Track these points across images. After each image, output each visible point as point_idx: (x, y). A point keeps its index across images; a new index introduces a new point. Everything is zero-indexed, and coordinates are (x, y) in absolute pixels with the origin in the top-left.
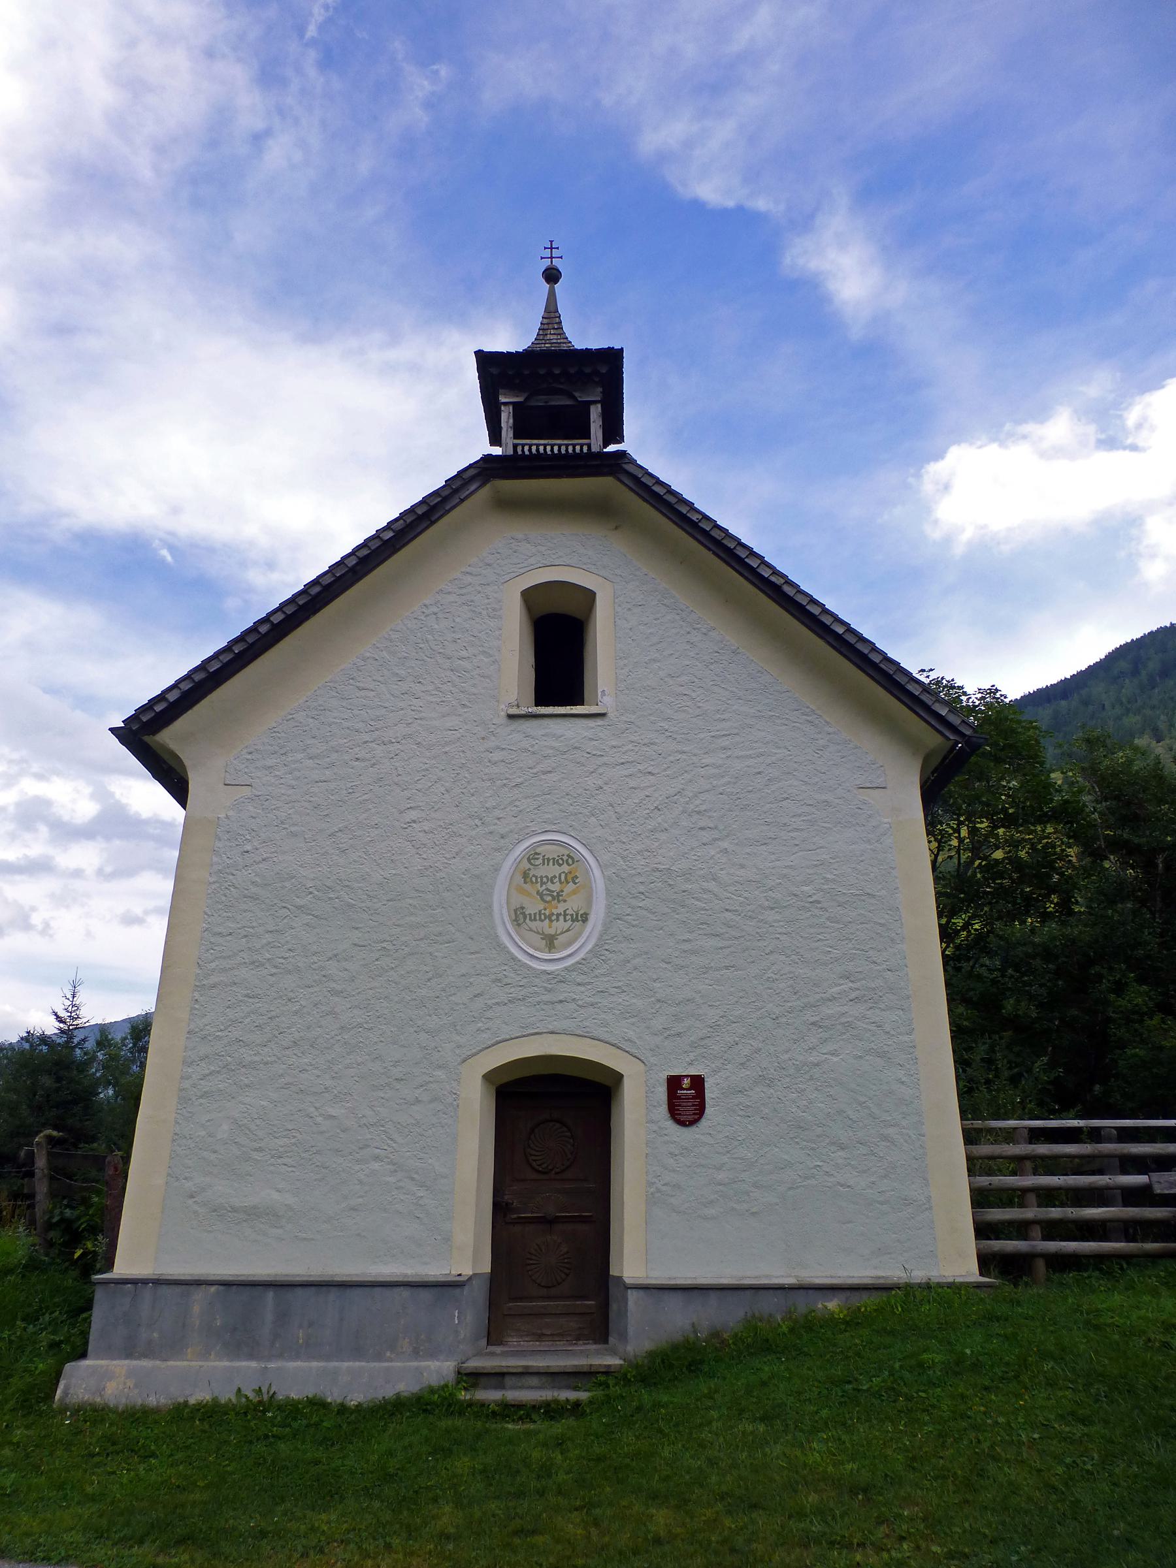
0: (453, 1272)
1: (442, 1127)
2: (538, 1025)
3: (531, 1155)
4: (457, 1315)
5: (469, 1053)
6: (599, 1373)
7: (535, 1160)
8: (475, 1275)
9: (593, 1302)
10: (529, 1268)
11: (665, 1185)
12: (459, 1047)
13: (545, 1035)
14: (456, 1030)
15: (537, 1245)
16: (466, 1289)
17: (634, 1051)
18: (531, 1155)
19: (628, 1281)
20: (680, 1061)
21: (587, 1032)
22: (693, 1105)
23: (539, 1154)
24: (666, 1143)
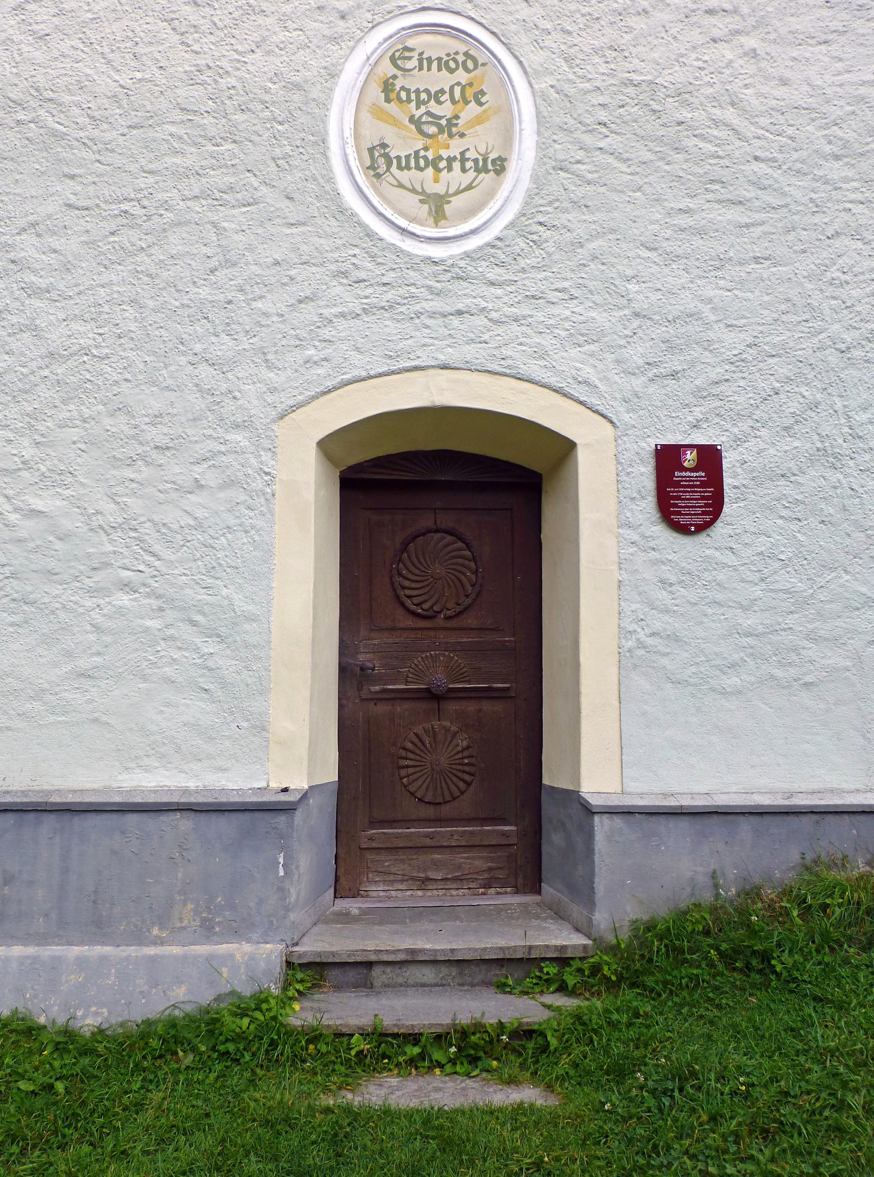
0: (275, 785)
1: (246, 532)
2: (418, 353)
3: (404, 588)
4: (281, 860)
5: (291, 402)
6: (544, 959)
7: (409, 597)
9: (513, 828)
10: (403, 772)
11: (653, 634)
12: (273, 390)
13: (431, 371)
14: (267, 361)
15: (415, 734)
16: (299, 815)
17: (593, 401)
18: (404, 588)
19: (594, 801)
21: (508, 367)
23: (421, 585)
24: (655, 563)
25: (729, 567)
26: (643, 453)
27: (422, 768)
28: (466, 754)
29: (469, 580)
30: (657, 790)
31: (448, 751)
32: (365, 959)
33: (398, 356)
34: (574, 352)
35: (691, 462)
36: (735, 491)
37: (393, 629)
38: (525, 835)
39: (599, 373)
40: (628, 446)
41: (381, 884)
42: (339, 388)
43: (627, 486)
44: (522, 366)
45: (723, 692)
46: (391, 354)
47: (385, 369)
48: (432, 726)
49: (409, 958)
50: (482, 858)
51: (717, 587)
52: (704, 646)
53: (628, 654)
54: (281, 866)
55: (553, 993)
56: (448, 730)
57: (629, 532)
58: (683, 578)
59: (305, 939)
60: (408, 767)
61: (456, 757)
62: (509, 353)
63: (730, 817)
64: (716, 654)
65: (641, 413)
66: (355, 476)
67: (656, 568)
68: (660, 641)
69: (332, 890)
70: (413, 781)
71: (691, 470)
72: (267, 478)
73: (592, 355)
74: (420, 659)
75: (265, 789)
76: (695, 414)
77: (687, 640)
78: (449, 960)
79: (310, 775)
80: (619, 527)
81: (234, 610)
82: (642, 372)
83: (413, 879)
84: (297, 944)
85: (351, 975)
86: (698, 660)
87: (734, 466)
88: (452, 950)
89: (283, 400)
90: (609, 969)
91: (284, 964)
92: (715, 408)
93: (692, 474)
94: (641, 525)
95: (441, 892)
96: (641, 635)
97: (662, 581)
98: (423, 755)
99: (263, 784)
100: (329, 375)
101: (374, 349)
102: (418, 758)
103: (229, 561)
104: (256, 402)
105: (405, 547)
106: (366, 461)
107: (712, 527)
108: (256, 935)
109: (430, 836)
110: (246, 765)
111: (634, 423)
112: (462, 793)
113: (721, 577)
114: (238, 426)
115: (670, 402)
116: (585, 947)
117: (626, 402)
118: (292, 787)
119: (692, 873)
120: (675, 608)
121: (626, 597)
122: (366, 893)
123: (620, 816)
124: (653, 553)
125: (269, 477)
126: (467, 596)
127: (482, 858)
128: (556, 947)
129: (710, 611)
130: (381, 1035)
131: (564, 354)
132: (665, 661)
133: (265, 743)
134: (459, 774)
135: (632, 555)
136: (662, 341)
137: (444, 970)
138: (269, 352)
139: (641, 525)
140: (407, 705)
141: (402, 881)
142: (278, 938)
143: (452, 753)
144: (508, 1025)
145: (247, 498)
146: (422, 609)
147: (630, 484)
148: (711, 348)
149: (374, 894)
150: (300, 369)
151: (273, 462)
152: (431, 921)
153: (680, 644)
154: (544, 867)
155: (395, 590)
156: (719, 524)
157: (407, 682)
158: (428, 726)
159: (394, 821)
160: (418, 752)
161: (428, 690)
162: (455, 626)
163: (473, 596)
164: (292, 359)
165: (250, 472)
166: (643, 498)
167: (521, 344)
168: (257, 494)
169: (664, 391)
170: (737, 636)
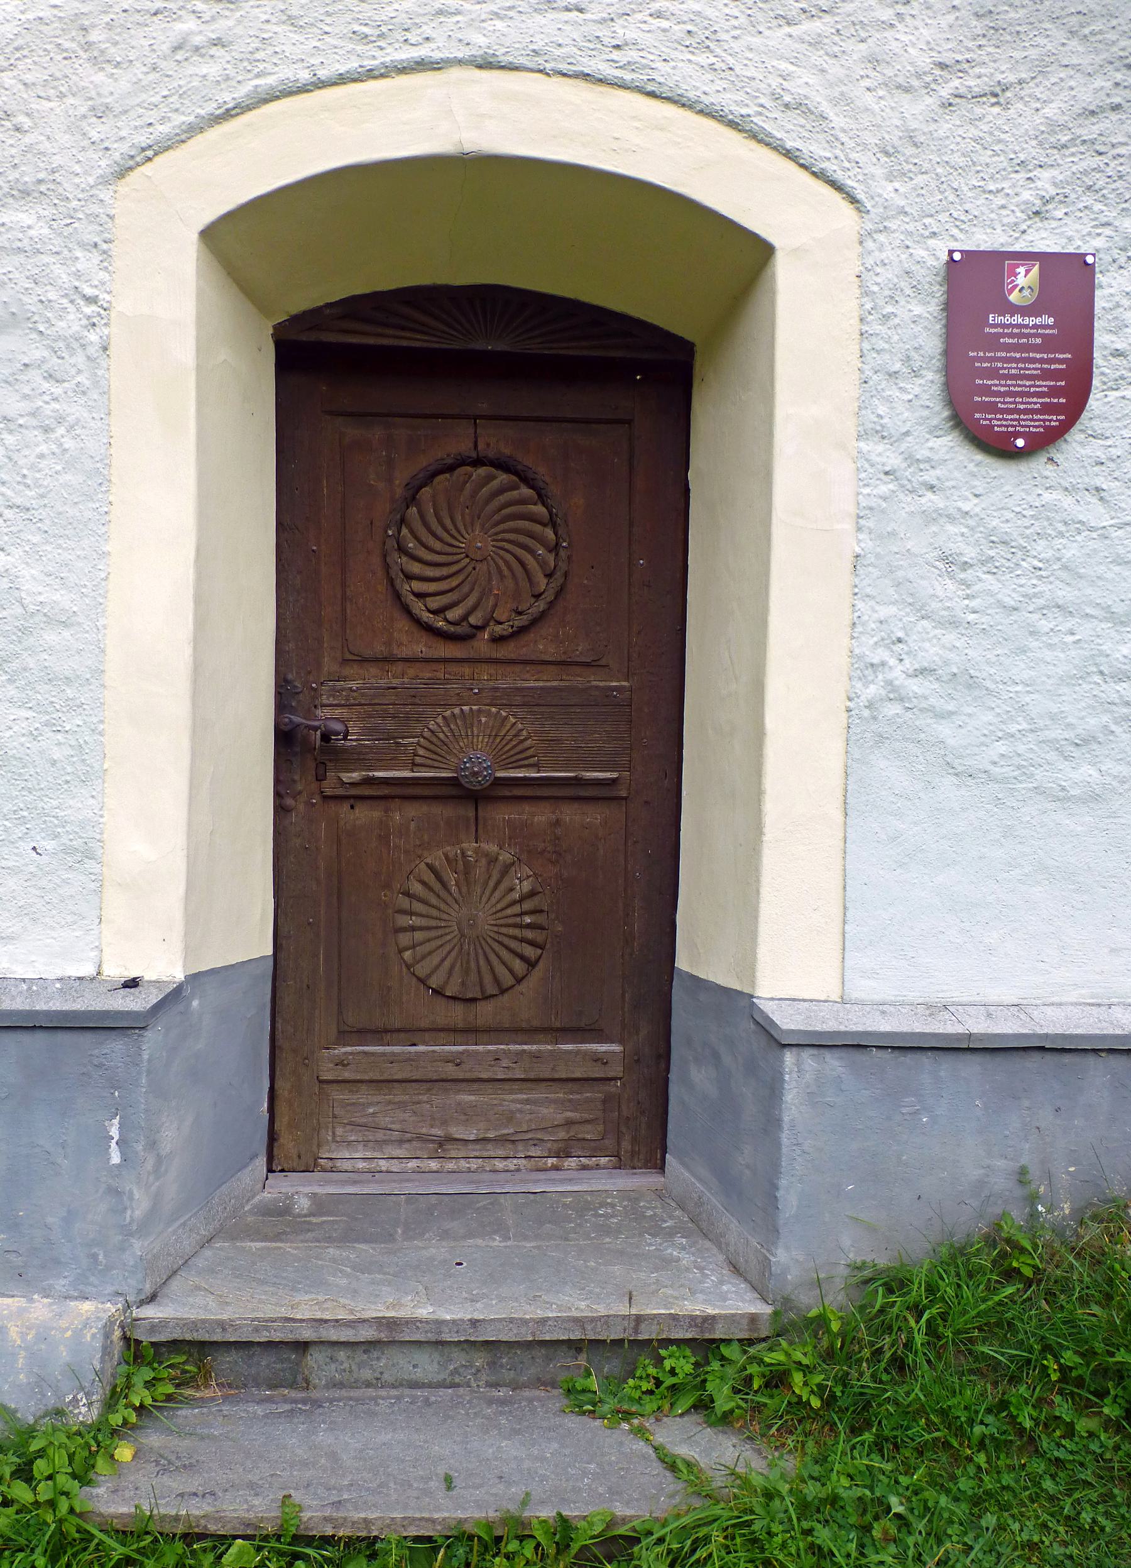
0: (116, 971)
1: (47, 430)
2: (427, 30)
3: (409, 577)
4: (114, 1132)
5: (142, 139)
6: (667, 1342)
7: (420, 596)
8: (194, 978)
9: (616, 1048)
10: (404, 939)
11: (921, 672)
12: (100, 113)
13: (455, 73)
14: (88, 46)
15: (430, 867)
16: (152, 1041)
17: (814, 149)
18: (409, 577)
19: (787, 1020)
20: (1000, 200)
21: (627, 66)
22: (1046, 375)
23: (445, 571)
24: (931, 517)
25: (1091, 529)
26: (920, 272)
27: (440, 932)
28: (527, 906)
29: (543, 564)
30: (913, 996)
31: (493, 900)
32: (290, 1337)
33: (382, 36)
34: (778, 36)
35: (1026, 293)
36: (1115, 361)
37: (388, 660)
38: (638, 1061)
39: (831, 85)
40: (888, 254)
41: (360, 1147)
42: (249, 108)
43: (882, 345)
44: (659, 65)
45: (1062, 798)
46: (366, 30)
47: (351, 65)
48: (463, 853)
49: (383, 1336)
50: (555, 1101)
51: (1064, 575)
52: (1028, 699)
53: (866, 713)
54: (113, 1144)
55: (682, 1415)
56: (492, 860)
57: (880, 448)
58: (992, 553)
59: (175, 1284)
60: (413, 929)
61: (509, 911)
62: (631, 34)
63: (1067, 1059)
64: (1053, 717)
65: (920, 180)
66: (304, 337)
67: (934, 529)
68: (936, 686)
69: (261, 1162)
70: (423, 957)
71: (1024, 311)
72: (89, 310)
73: (816, 43)
74: (440, 720)
75: (93, 979)
76: (1039, 184)
77: (992, 686)
78: (466, 1341)
79: (189, 951)
80: (859, 437)
81: (20, 601)
82: (927, 86)
83: (420, 1138)
84: (152, 1298)
85: (265, 1362)
86: (1013, 728)
87: (1118, 305)
88: (474, 1323)
89: (123, 133)
90: (806, 1384)
91: (118, 1345)
92: (1085, 173)
93: (1027, 321)
94: (907, 433)
95: (474, 1164)
96: (897, 674)
97: (946, 559)
98: (443, 906)
99: (88, 970)
100: (228, 78)
101: (328, 20)
102: (435, 913)
103: (9, 493)
104: (65, 139)
105: (412, 498)
106: (329, 305)
107: (1060, 442)
108: (62, 1282)
109: (456, 1061)
110: (53, 928)
111: (902, 203)
112: (519, 981)
113: (1072, 552)
114: (26, 193)
115: (985, 157)
116: (753, 1319)
117: (887, 154)
118: (149, 976)
119: (982, 1171)
120: (971, 617)
121: (868, 590)
122: (330, 1164)
123: (837, 1053)
124: (929, 495)
125: (94, 308)
126: (537, 596)
127: (555, 1101)
128: (693, 1318)
129: (1045, 625)
130: (296, 1539)
131: (756, 41)
132: (944, 730)
133: (93, 886)
134: (514, 944)
135: (885, 499)
136: (977, 15)
137: (459, 1358)
138: (94, 26)
139: (907, 433)
140: (413, 810)
141: (401, 1142)
142: (110, 1289)
143: (499, 906)
144: (582, 1524)
145: (46, 353)
146: (446, 620)
147: (888, 341)
148: (1086, 31)
149: (347, 1165)
150: (163, 64)
151: (103, 275)
152: (445, 1235)
153: (977, 693)
154: (670, 1127)
155: (391, 582)
156: (1075, 435)
157: (414, 764)
158: (453, 851)
159: (386, 1031)
160: (434, 900)
161: (454, 782)
162: (513, 656)
163: (549, 596)
164: (146, 43)
165: (52, 295)
166: (916, 373)
167: (658, 15)
168: (68, 346)
169: (973, 132)
170: (1097, 678)
